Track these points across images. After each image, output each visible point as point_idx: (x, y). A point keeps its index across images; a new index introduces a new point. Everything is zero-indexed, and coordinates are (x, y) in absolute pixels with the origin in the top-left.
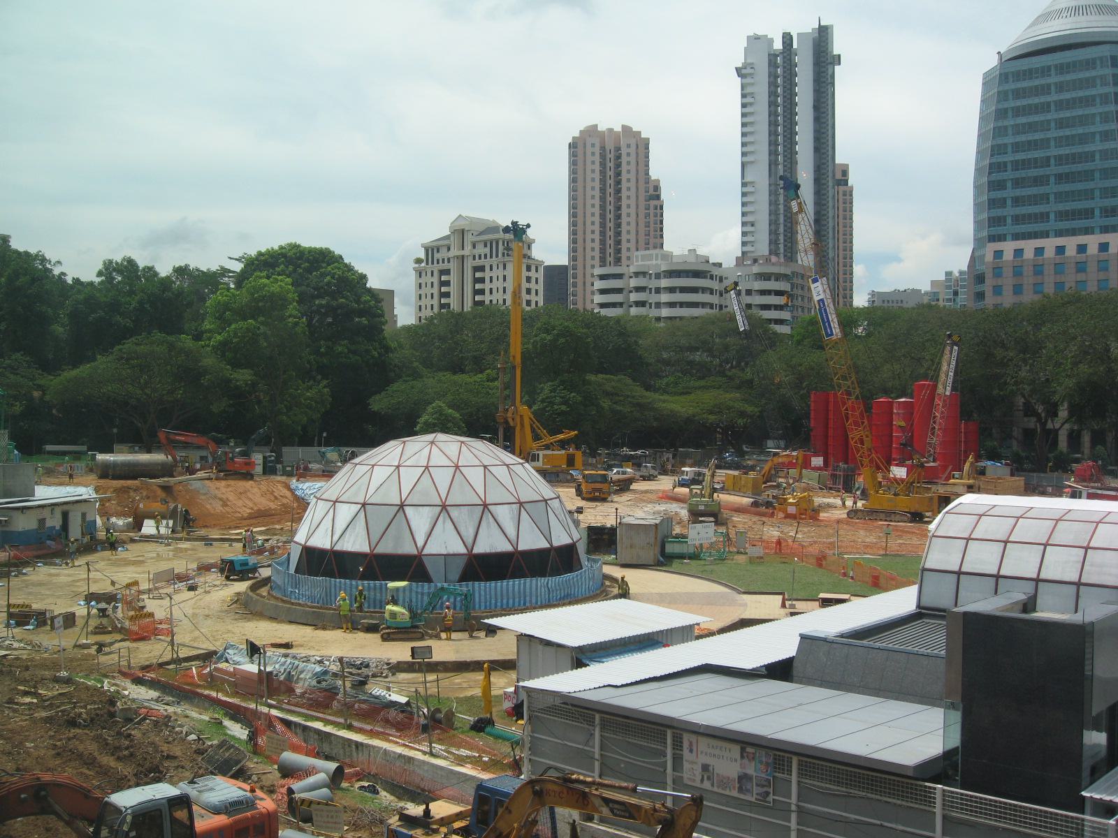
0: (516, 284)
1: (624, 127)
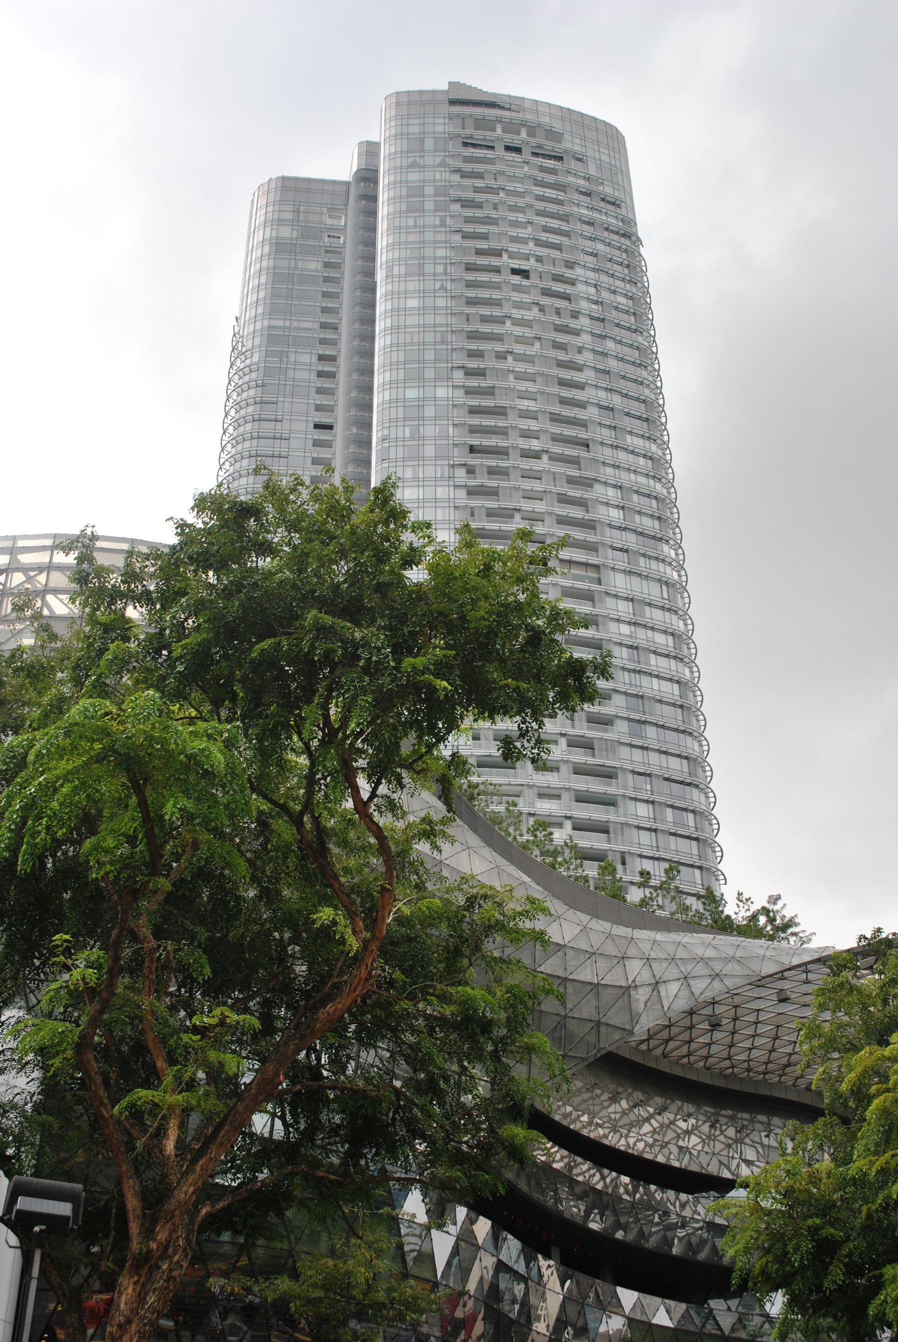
0: (502, 105)
1: (450, 83)
